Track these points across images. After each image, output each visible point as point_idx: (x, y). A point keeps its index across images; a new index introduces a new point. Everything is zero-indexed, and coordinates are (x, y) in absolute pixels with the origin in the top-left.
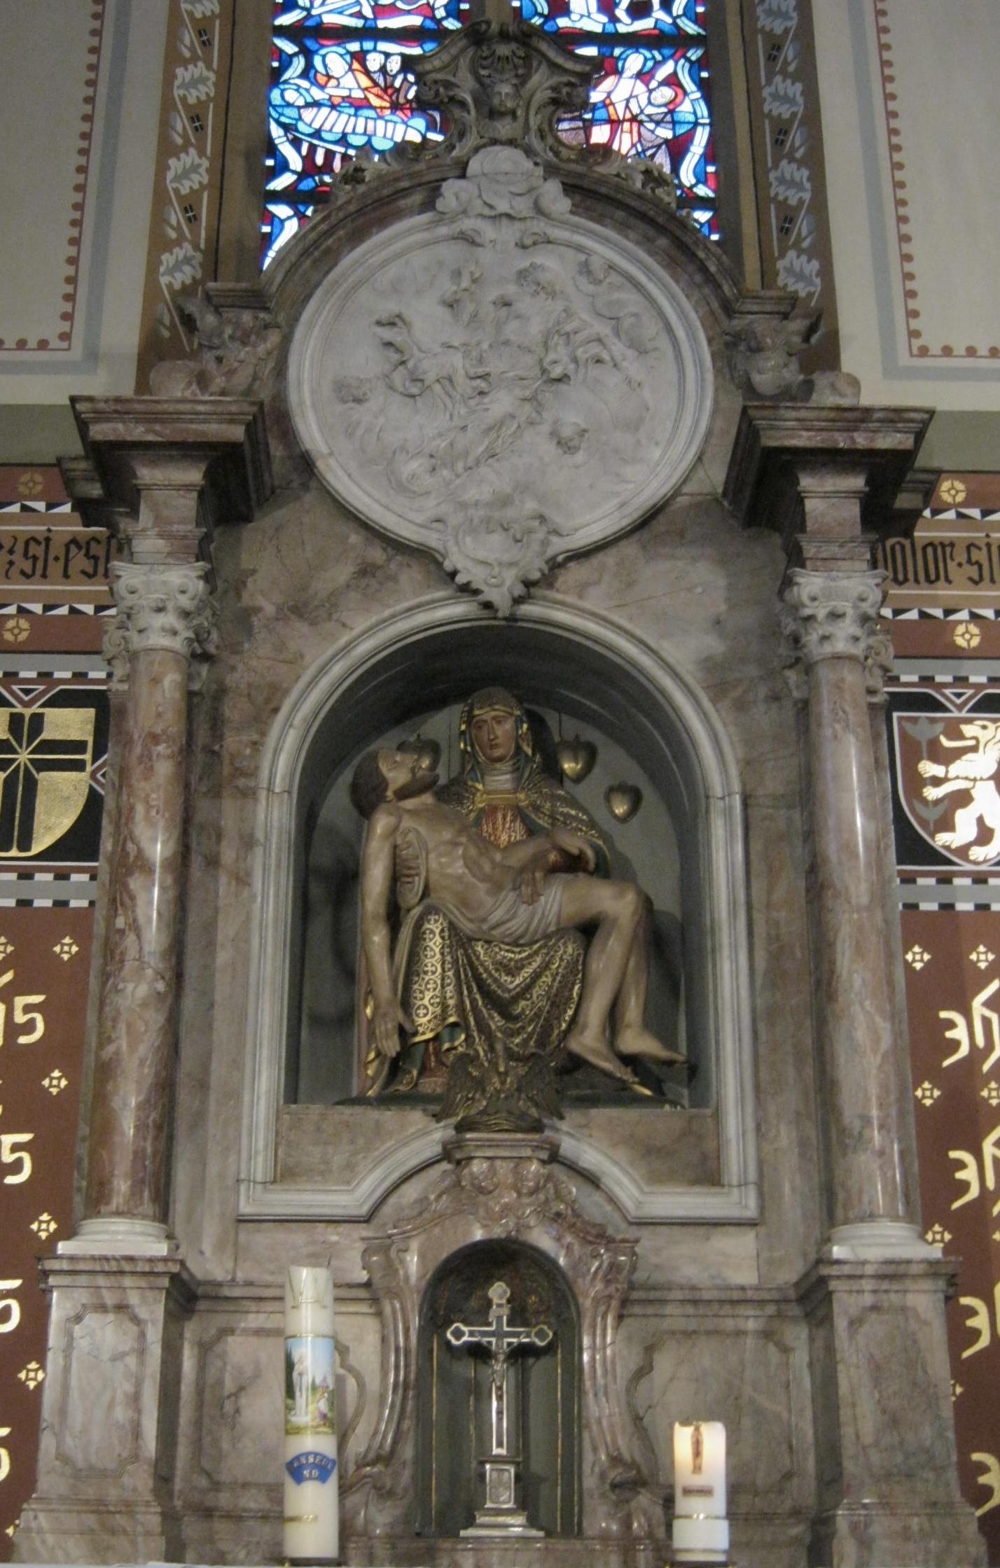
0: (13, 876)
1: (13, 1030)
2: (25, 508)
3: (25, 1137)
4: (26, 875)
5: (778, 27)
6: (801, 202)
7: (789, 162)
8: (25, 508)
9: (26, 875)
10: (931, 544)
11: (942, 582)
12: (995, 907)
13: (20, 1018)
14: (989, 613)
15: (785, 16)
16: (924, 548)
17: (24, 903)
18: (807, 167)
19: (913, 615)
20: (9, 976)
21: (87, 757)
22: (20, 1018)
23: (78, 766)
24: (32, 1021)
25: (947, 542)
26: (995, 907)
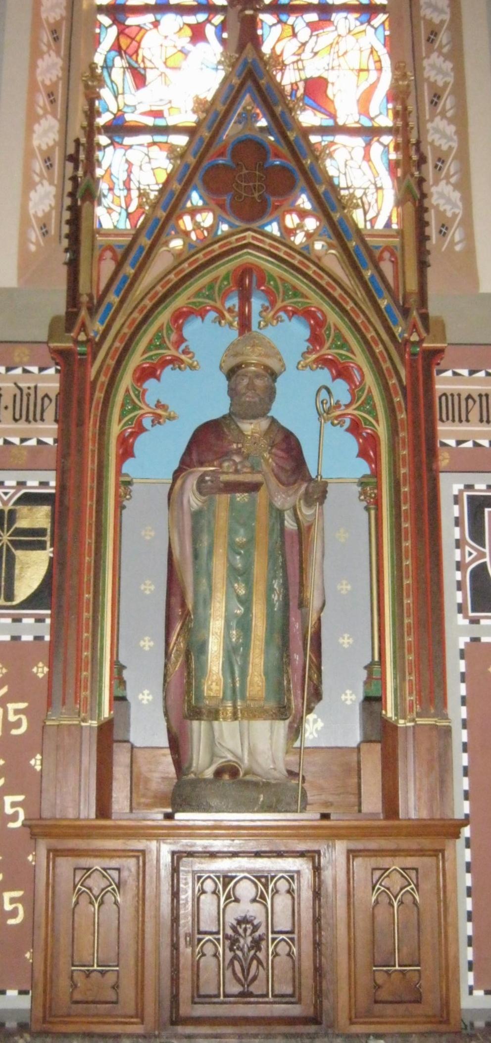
0: (9, 621)
1: (8, 725)
2: (455, 374)
3: (20, 798)
4: (17, 620)
5: (436, 19)
6: (450, 148)
7: (441, 119)
8: (455, 374)
9: (17, 620)
10: (445, 394)
11: (450, 421)
12: (484, 639)
13: (12, 718)
14: (485, 443)
15: (441, 11)
16: (440, 398)
17: (16, 638)
18: (455, 124)
19: (469, 444)
20: (5, 690)
21: (47, 538)
22: (12, 718)
23: (41, 546)
24: (20, 720)
25: (483, 393)
26: (484, 639)
